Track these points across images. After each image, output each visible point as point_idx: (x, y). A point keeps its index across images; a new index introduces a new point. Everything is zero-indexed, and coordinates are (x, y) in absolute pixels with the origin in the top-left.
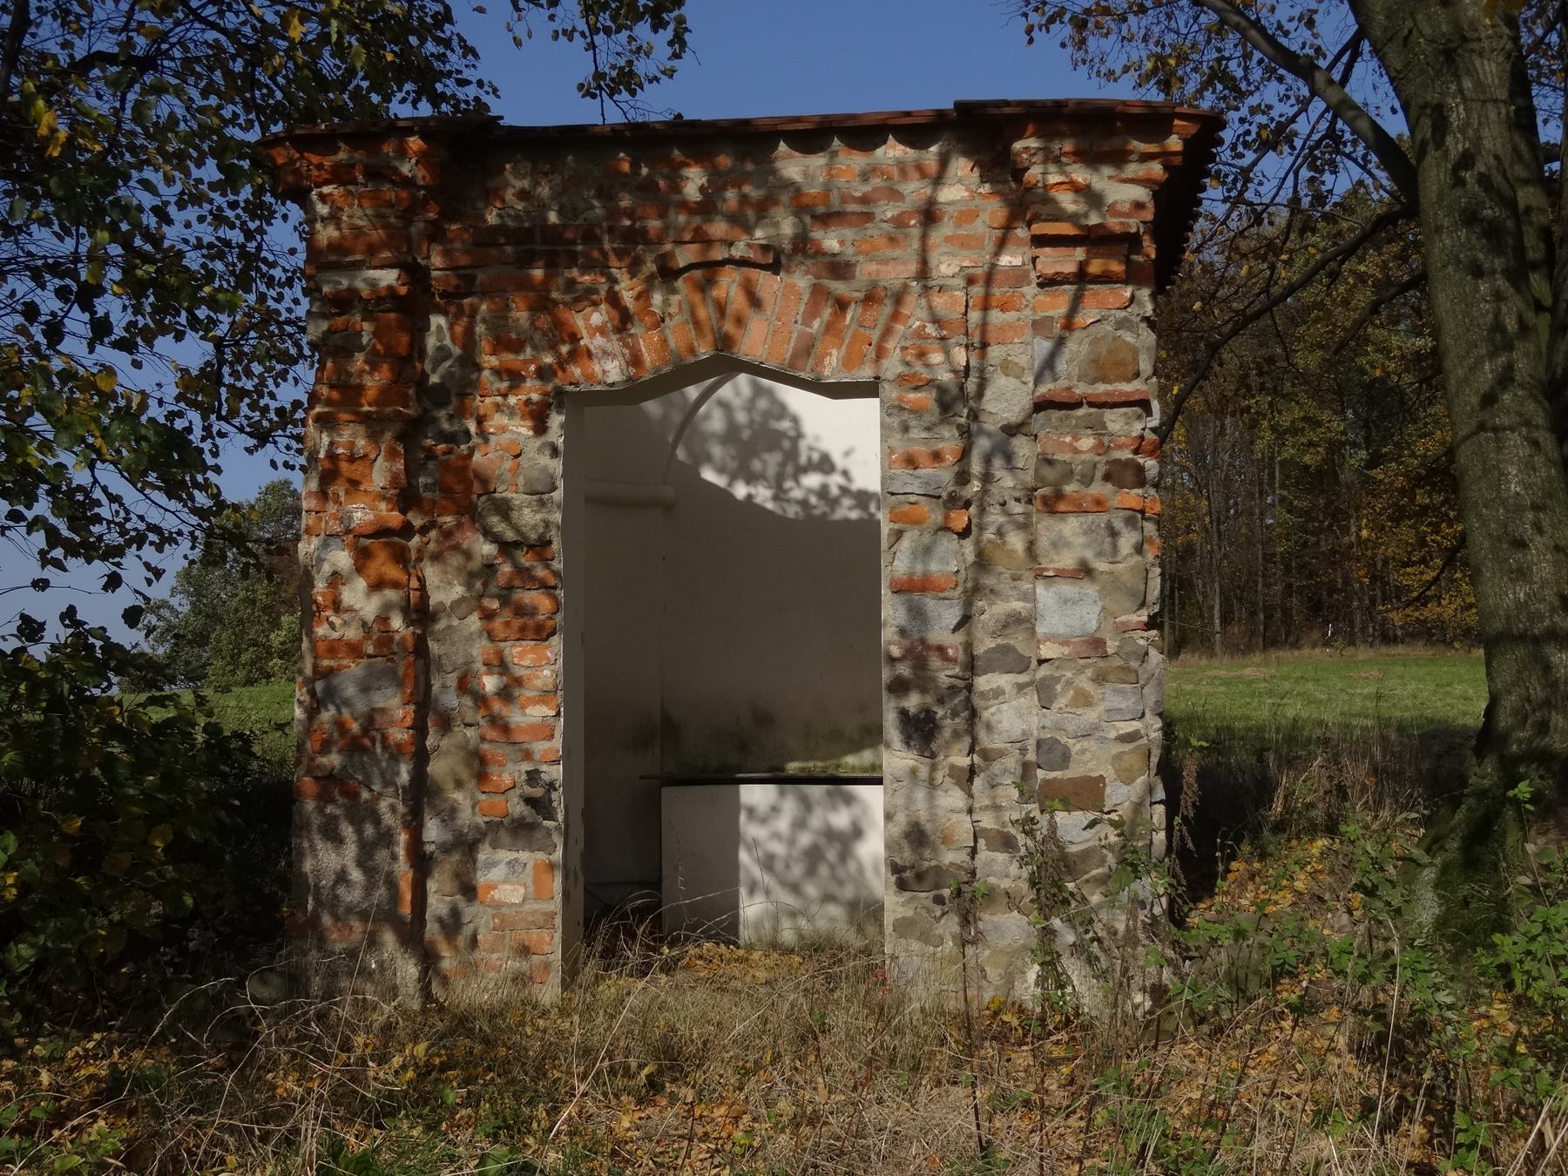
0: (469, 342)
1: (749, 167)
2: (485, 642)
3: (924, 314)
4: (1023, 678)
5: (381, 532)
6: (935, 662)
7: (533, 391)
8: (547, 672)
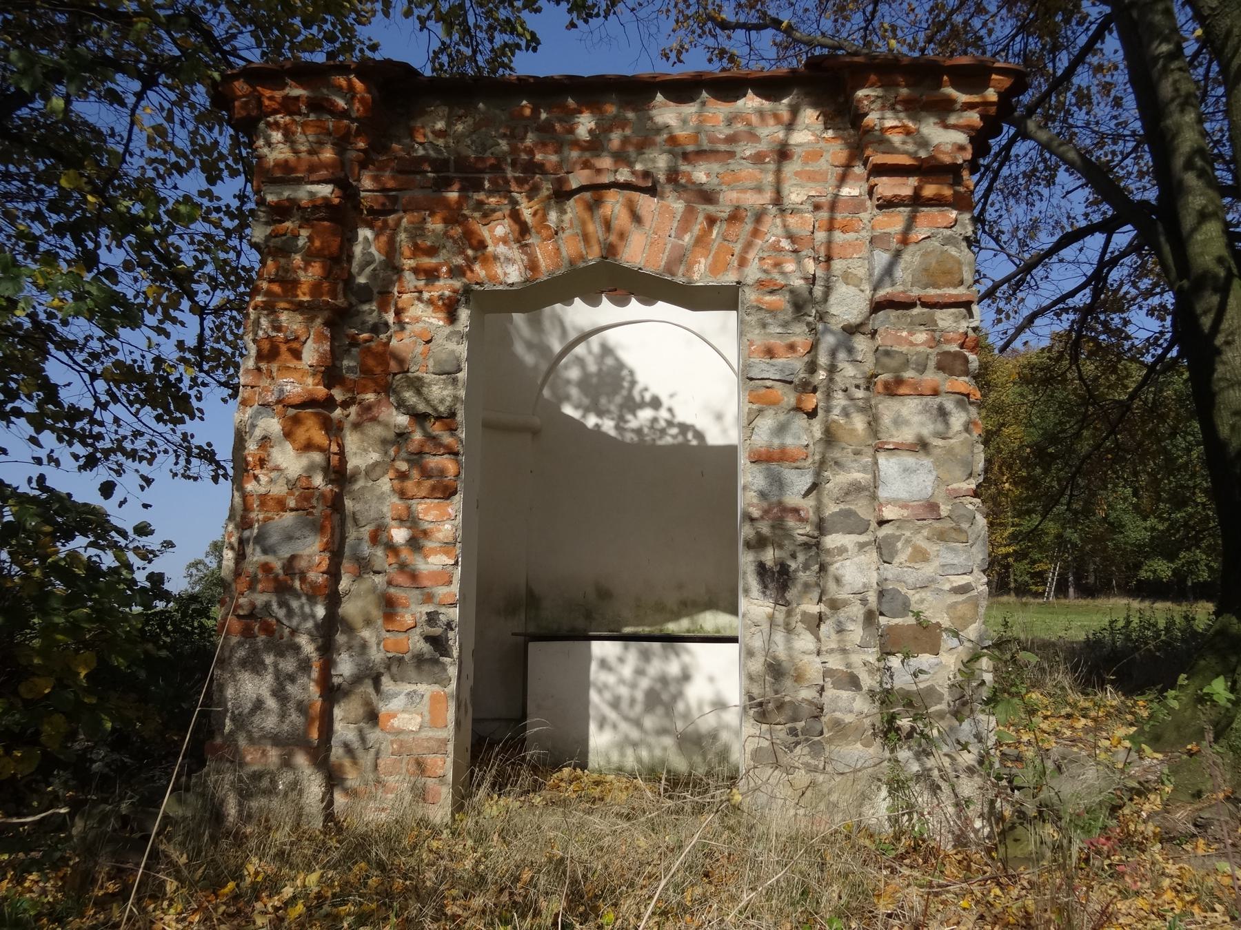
0: (391, 250)
1: (630, 115)
2: (395, 499)
3: (780, 231)
4: (863, 538)
5: (310, 403)
6: (791, 522)
7: (445, 286)
8: (448, 526)
